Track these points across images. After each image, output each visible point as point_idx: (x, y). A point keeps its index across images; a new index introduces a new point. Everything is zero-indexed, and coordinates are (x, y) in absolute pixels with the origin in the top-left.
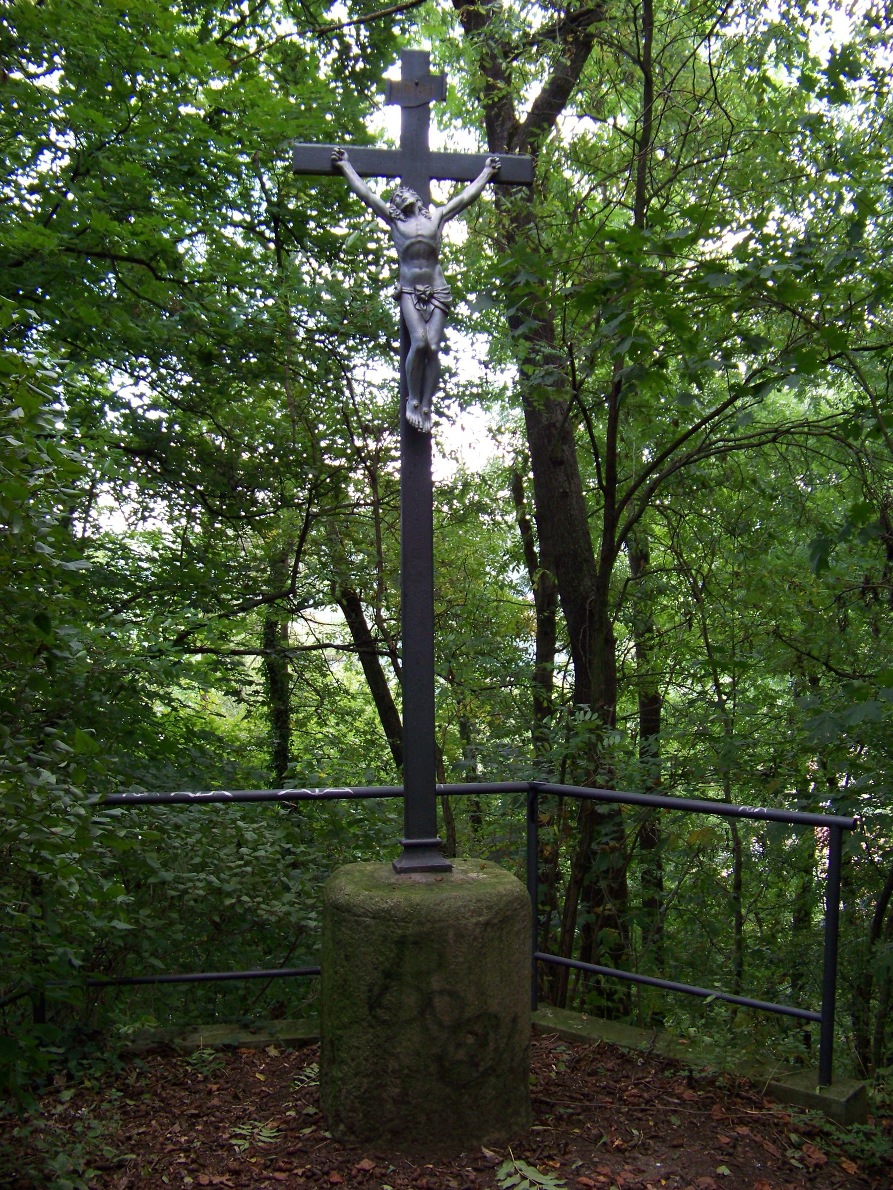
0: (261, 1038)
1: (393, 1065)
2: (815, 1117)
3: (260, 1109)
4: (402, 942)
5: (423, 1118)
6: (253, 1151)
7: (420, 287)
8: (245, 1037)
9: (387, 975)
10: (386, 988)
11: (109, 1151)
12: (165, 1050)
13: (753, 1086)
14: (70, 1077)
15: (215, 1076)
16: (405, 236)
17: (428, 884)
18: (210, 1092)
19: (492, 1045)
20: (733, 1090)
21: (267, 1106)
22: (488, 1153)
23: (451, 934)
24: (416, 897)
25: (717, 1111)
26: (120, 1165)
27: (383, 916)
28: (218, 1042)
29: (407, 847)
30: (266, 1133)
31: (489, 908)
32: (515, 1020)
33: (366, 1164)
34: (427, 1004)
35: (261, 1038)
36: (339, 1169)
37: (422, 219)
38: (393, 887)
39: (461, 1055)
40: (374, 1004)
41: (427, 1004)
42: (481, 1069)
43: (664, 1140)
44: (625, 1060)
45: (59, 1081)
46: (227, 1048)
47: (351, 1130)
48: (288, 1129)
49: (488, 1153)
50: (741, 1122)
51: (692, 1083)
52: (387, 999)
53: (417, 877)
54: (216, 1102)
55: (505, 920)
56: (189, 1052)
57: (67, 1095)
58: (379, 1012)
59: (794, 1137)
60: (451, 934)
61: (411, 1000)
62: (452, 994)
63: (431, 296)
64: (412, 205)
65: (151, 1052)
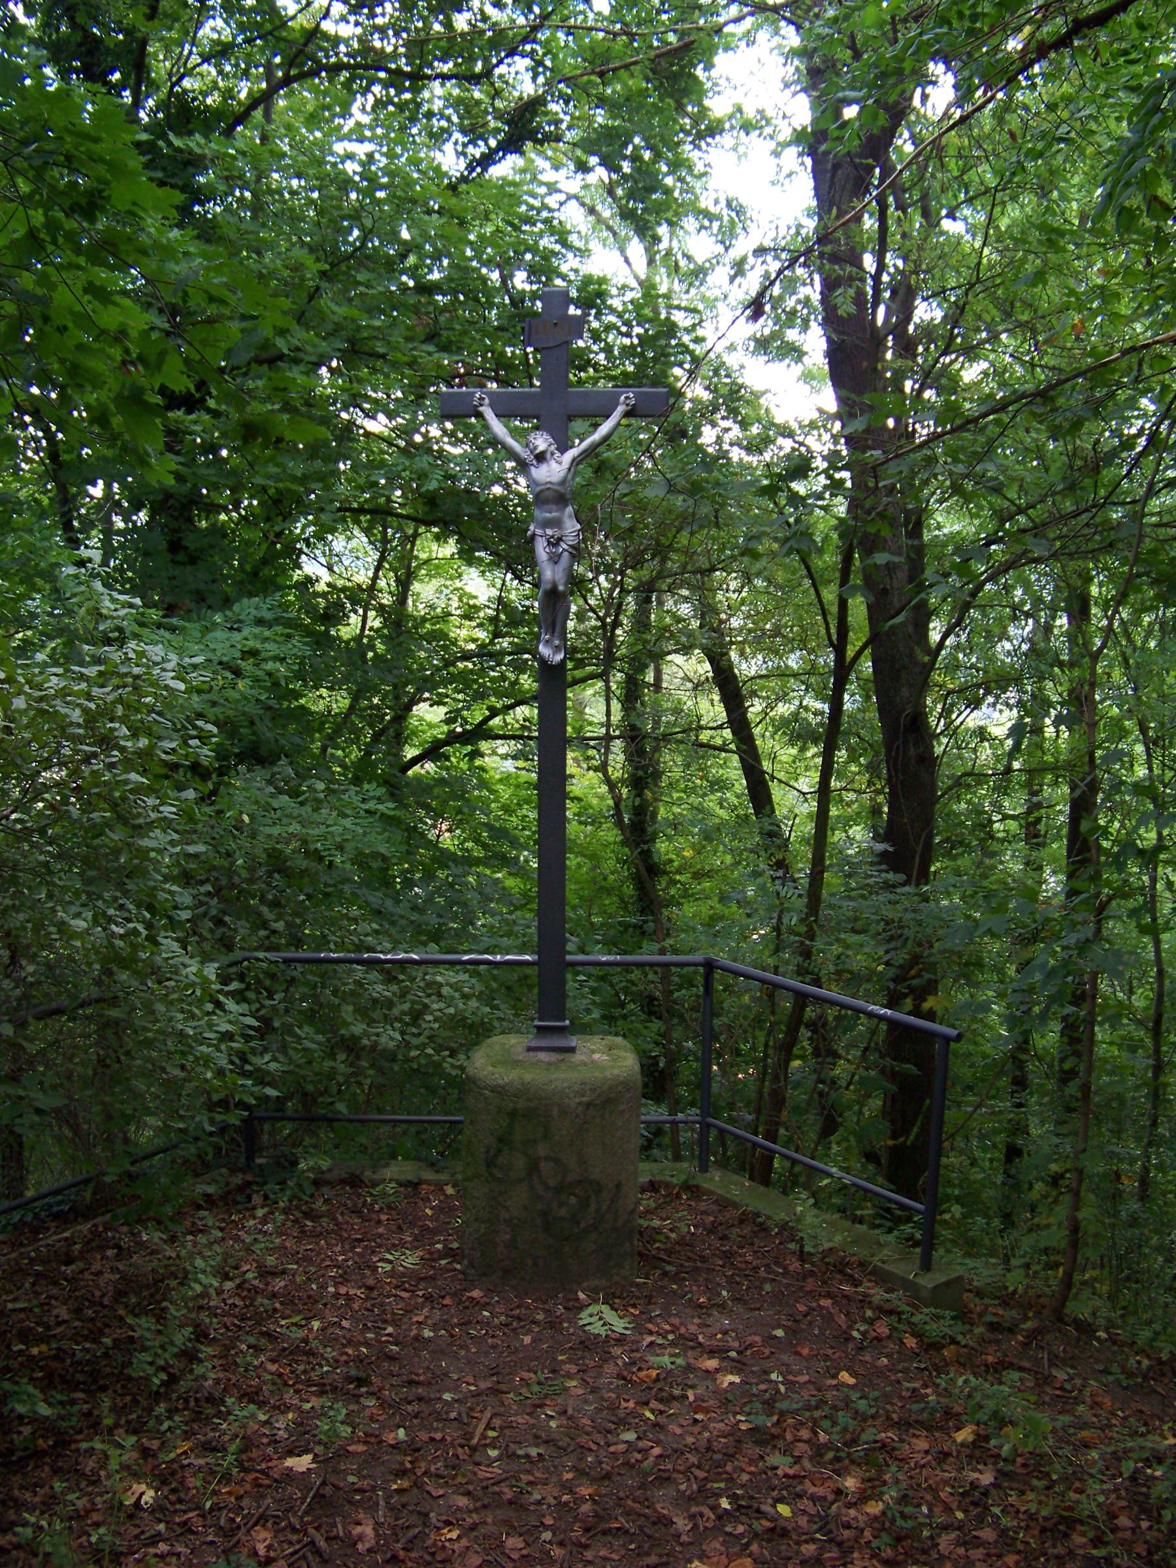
0: (442, 1177)
1: (504, 1215)
2: (897, 1299)
3: (416, 1239)
4: (513, 1114)
5: (529, 1262)
6: (392, 1274)
7: (549, 532)
8: (428, 1175)
9: (501, 1140)
10: (499, 1151)
11: (271, 1261)
12: (354, 1181)
13: (862, 1264)
14: (266, 1197)
15: (389, 1208)
16: (537, 484)
17: (549, 1064)
18: (379, 1222)
19: (593, 1207)
20: (841, 1268)
21: (424, 1237)
22: (581, 1295)
23: (555, 1112)
24: (528, 1077)
25: (810, 1284)
26: (283, 1272)
27: (500, 1091)
28: (402, 1178)
29: (539, 1028)
30: (410, 1260)
31: (593, 1090)
32: (619, 1186)
33: (476, 1293)
34: (533, 1168)
35: (442, 1177)
36: (454, 1295)
37: (553, 464)
38: (517, 1063)
39: (563, 1212)
40: (490, 1163)
41: (533, 1168)
42: (583, 1224)
43: (745, 1302)
44: (763, 1228)
45: (257, 1199)
46: (409, 1183)
47: (471, 1265)
48: (430, 1259)
49: (581, 1295)
50: (829, 1295)
51: (803, 1257)
52: (501, 1160)
53: (543, 1056)
54: (381, 1230)
55: (608, 1101)
56: (374, 1184)
57: (260, 1213)
58: (495, 1171)
59: (869, 1313)
60: (555, 1112)
61: (520, 1162)
62: (557, 1161)
63: (560, 539)
64: (543, 453)
65: (343, 1182)
